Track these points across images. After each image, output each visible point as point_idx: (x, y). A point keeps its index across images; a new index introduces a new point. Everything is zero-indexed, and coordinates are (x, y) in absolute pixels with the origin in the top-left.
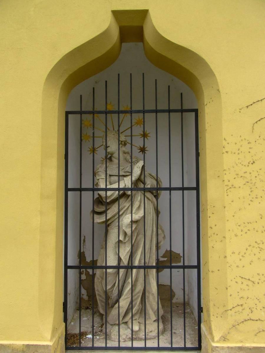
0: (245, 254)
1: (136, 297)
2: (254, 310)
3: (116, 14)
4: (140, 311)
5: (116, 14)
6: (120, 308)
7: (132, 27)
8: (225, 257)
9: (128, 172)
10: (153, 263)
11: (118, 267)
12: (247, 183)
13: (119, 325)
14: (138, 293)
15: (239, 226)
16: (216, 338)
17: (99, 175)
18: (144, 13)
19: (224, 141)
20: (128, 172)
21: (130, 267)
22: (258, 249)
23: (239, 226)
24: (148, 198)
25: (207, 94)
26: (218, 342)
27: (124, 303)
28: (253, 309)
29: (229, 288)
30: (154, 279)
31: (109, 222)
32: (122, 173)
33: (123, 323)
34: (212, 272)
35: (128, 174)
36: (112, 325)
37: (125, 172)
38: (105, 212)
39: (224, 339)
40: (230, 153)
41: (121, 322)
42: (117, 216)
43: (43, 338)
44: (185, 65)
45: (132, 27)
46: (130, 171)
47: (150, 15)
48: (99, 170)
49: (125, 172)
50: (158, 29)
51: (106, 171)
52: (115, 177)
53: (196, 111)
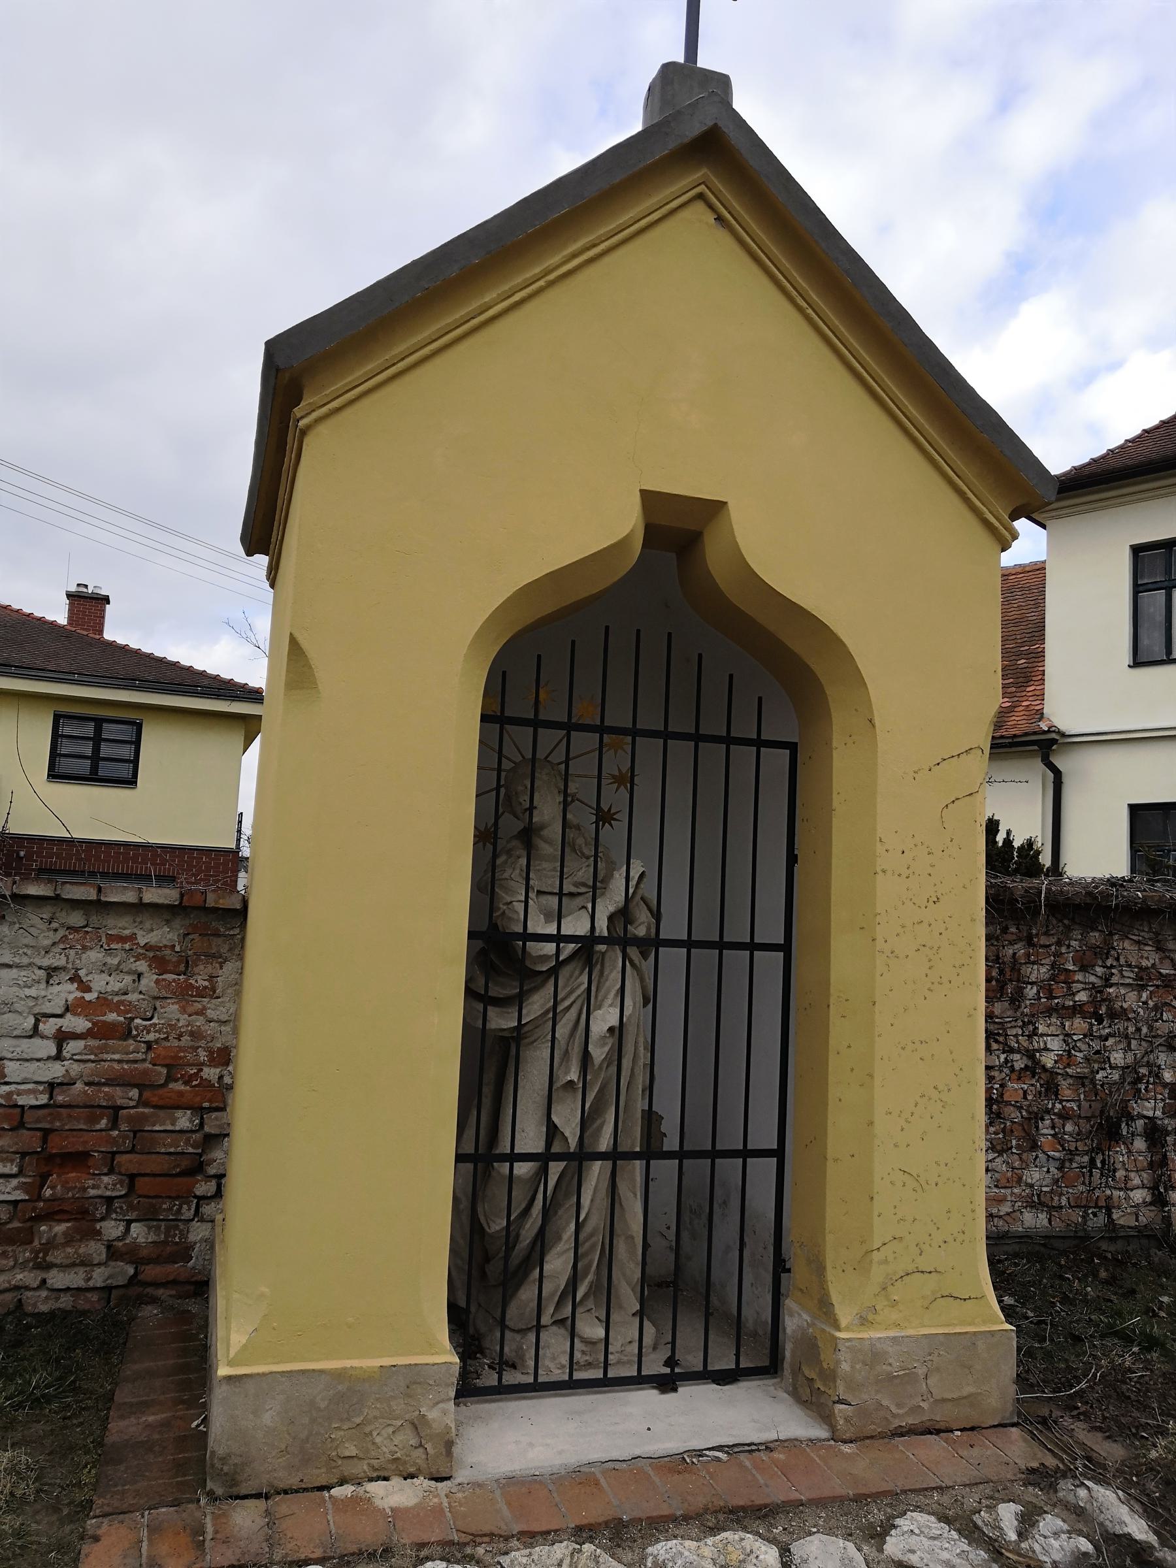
0: (912, 1114)
1: (587, 1245)
2: (925, 1247)
3: (649, 498)
4: (556, 1299)
5: (649, 498)
6: (545, 1280)
7: (678, 532)
8: (871, 1123)
9: (584, 885)
10: (633, 1145)
11: (543, 1159)
12: (922, 948)
13: (539, 1328)
14: (591, 1235)
15: (903, 1048)
16: (843, 1323)
17: (507, 890)
18: (715, 508)
19: (878, 844)
20: (584, 885)
21: (581, 1157)
22: (940, 1104)
23: (903, 1048)
24: (631, 962)
25: (840, 720)
26: (847, 1329)
27: (558, 1264)
28: (923, 1247)
29: (876, 1197)
30: (635, 1195)
31: (526, 1029)
32: (568, 887)
33: (555, 1323)
34: (836, 1160)
35: (583, 890)
36: (518, 1331)
37: (576, 885)
38: (519, 1001)
39: (864, 1322)
40: (889, 873)
41: (546, 1320)
42: (551, 1015)
43: (431, 1346)
44: (797, 646)
45: (678, 532)
46: (591, 884)
47: (729, 515)
48: (506, 875)
49: (576, 885)
50: (748, 560)
51: (528, 879)
52: (550, 897)
53: (793, 747)
